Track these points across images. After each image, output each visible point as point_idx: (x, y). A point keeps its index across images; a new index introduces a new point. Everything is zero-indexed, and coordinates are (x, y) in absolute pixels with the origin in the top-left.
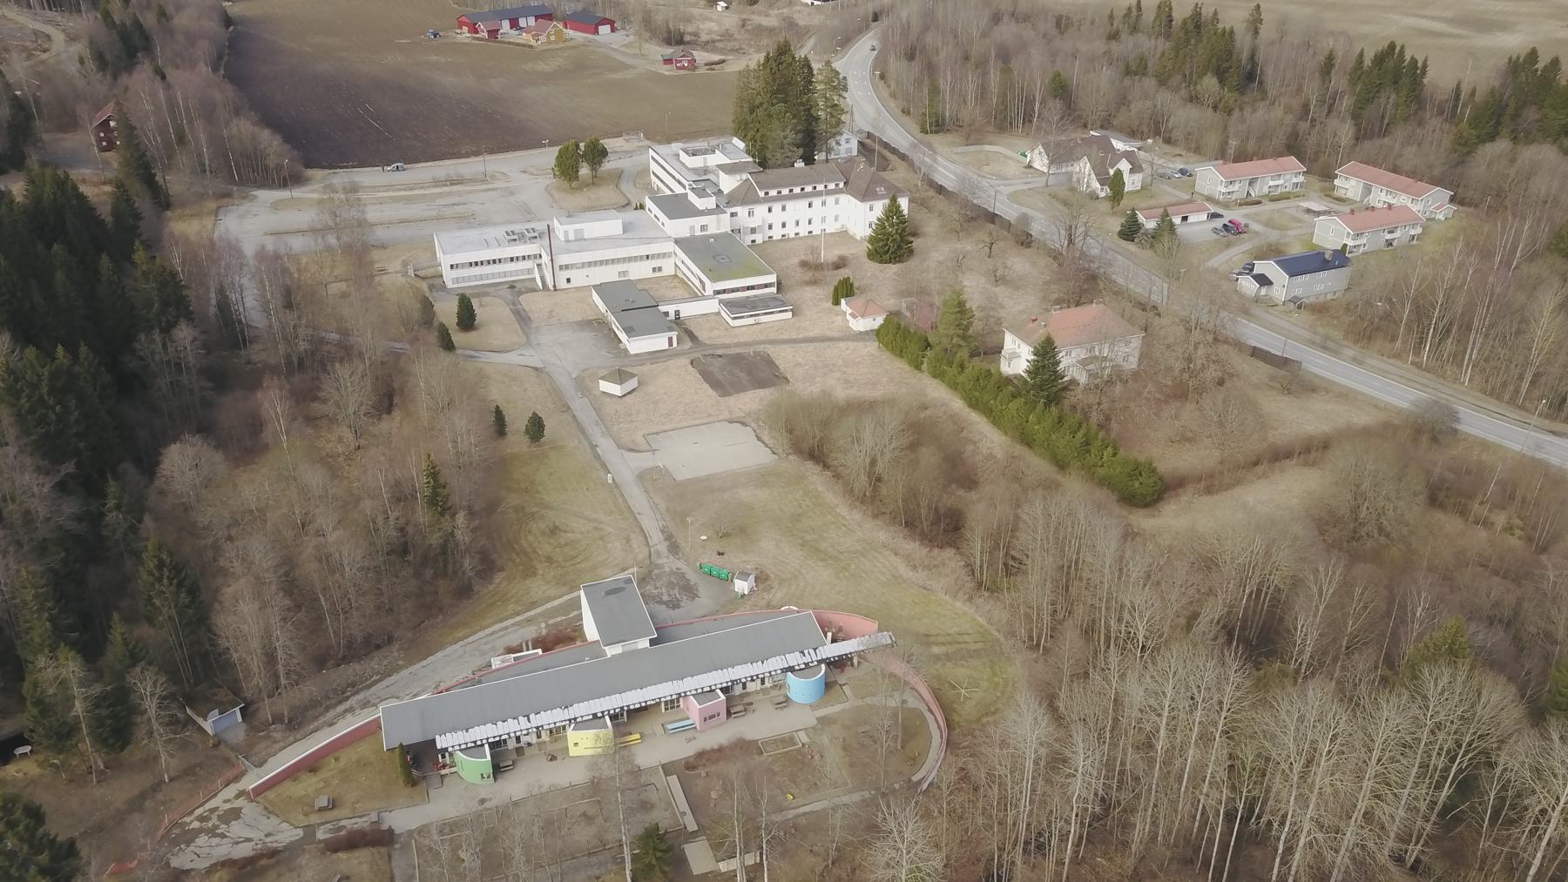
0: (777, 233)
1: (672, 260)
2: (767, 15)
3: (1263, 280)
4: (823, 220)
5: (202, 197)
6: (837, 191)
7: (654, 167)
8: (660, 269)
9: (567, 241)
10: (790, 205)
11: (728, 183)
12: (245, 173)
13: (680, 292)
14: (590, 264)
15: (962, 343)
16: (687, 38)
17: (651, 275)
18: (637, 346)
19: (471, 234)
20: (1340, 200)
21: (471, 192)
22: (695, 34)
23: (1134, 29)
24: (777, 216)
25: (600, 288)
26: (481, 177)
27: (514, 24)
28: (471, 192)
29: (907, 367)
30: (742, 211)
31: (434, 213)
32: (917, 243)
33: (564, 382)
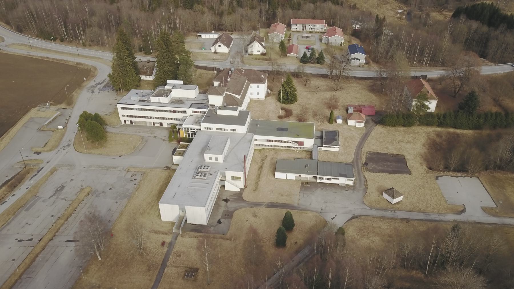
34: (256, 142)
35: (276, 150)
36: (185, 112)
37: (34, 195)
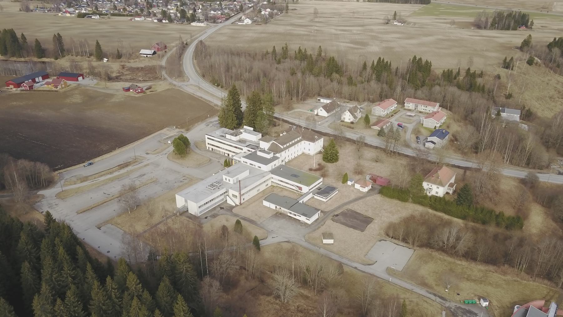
9: (234, 183)
34: (273, 180)
35: (283, 189)
36: (242, 149)
37: (128, 174)
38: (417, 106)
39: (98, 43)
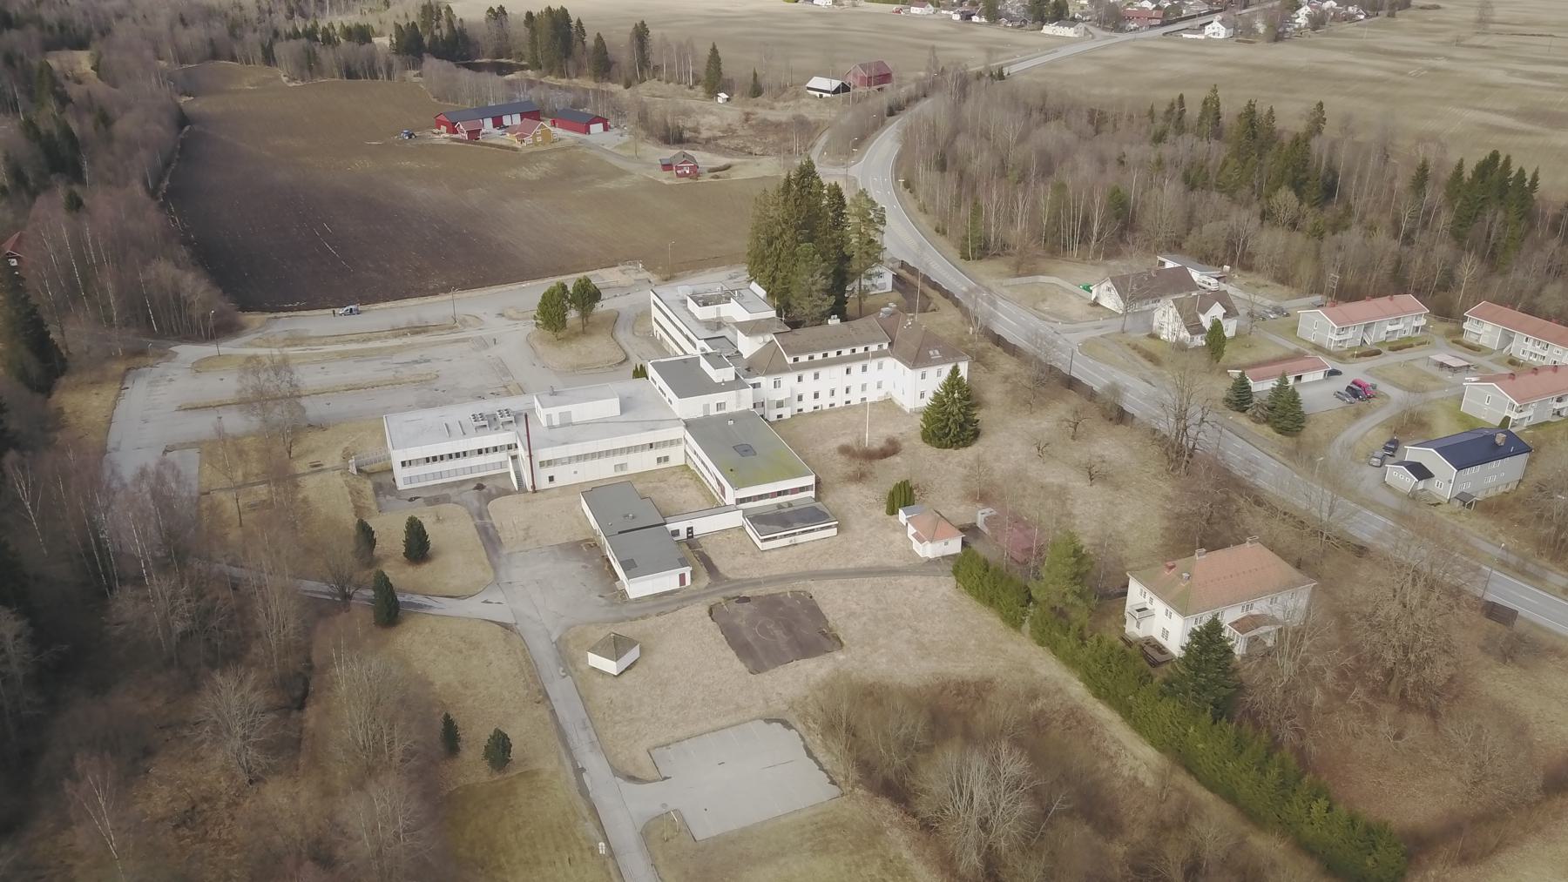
0: (808, 406)
1: (681, 448)
2: (772, 108)
3: (1420, 471)
4: (864, 387)
5: (110, 357)
6: (880, 354)
7: (655, 313)
8: (666, 459)
9: (551, 427)
10: (823, 372)
11: (748, 346)
12: (159, 324)
13: (691, 495)
14: (578, 458)
15: (1079, 602)
16: (687, 135)
17: (654, 466)
18: (638, 587)
19: (430, 416)
20: (1474, 349)
21: (435, 344)
22: (696, 130)
23: (1181, 129)
24: (809, 384)
25: (593, 492)
26: (450, 322)
27: (498, 123)
28: (435, 344)
29: (998, 621)
30: (766, 382)
31: (389, 375)
32: (981, 415)
33: (542, 649)
38: (1508, 338)
39: (714, 50)
